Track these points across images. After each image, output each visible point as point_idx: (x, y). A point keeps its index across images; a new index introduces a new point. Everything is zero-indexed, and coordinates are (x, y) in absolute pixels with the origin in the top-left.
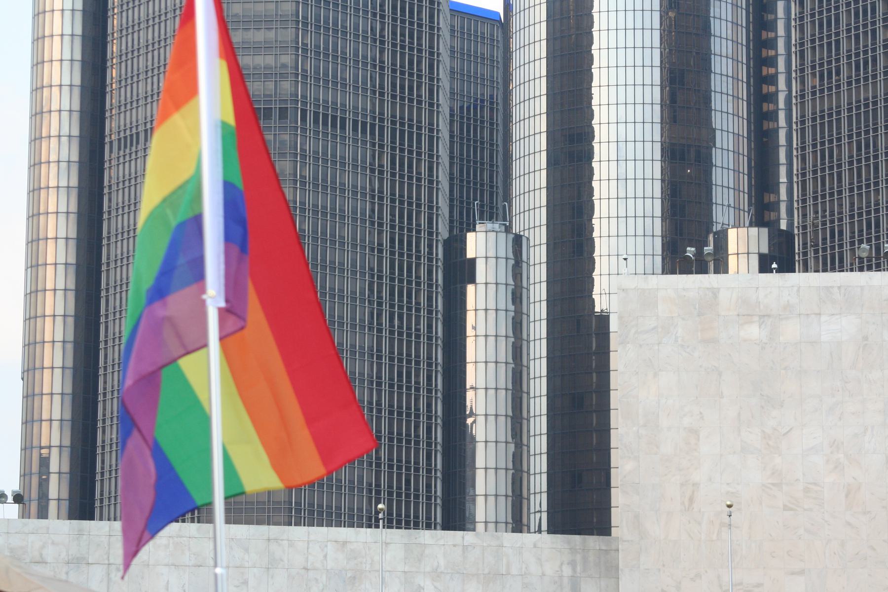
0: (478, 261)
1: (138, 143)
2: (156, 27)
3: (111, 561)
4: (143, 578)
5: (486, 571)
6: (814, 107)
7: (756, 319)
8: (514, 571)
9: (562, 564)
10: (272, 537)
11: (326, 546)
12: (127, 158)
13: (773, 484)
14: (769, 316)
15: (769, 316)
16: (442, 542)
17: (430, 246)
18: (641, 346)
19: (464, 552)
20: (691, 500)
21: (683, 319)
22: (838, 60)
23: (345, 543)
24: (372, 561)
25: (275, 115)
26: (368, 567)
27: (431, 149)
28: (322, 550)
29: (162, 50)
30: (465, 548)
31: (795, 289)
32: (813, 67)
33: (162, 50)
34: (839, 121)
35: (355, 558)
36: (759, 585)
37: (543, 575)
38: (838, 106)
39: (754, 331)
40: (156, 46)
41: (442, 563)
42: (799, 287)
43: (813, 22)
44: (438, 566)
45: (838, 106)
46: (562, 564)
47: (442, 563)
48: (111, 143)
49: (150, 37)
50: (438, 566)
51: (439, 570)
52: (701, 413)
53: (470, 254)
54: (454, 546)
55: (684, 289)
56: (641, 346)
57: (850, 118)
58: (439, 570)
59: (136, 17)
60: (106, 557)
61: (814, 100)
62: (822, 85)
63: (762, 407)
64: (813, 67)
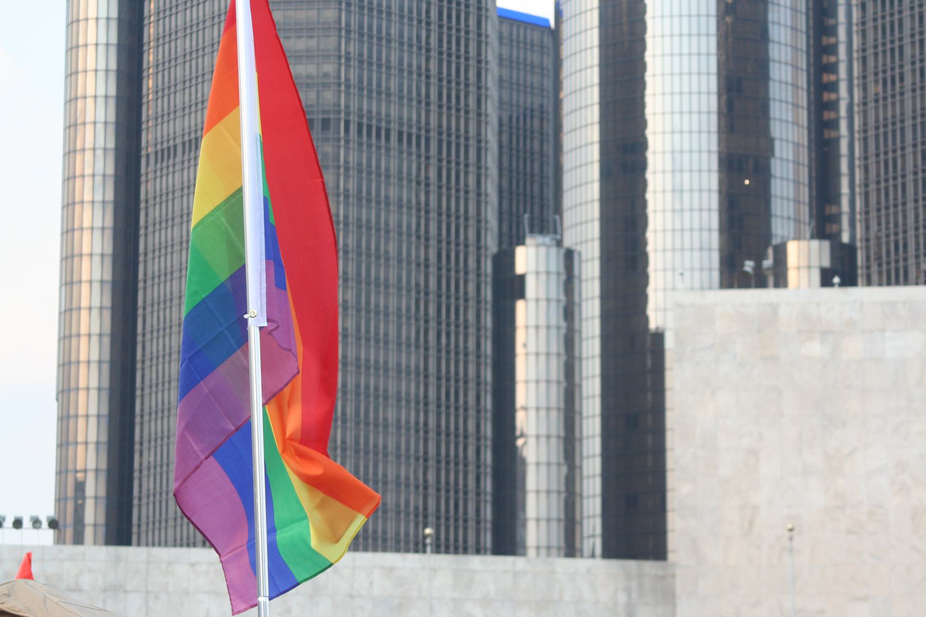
1: (175, 155)
6: (877, 115)
20: (751, 523)
30: (516, 574)
32: (876, 74)
39: (815, 348)
61: (877, 108)
62: (885, 91)
64: (876, 74)
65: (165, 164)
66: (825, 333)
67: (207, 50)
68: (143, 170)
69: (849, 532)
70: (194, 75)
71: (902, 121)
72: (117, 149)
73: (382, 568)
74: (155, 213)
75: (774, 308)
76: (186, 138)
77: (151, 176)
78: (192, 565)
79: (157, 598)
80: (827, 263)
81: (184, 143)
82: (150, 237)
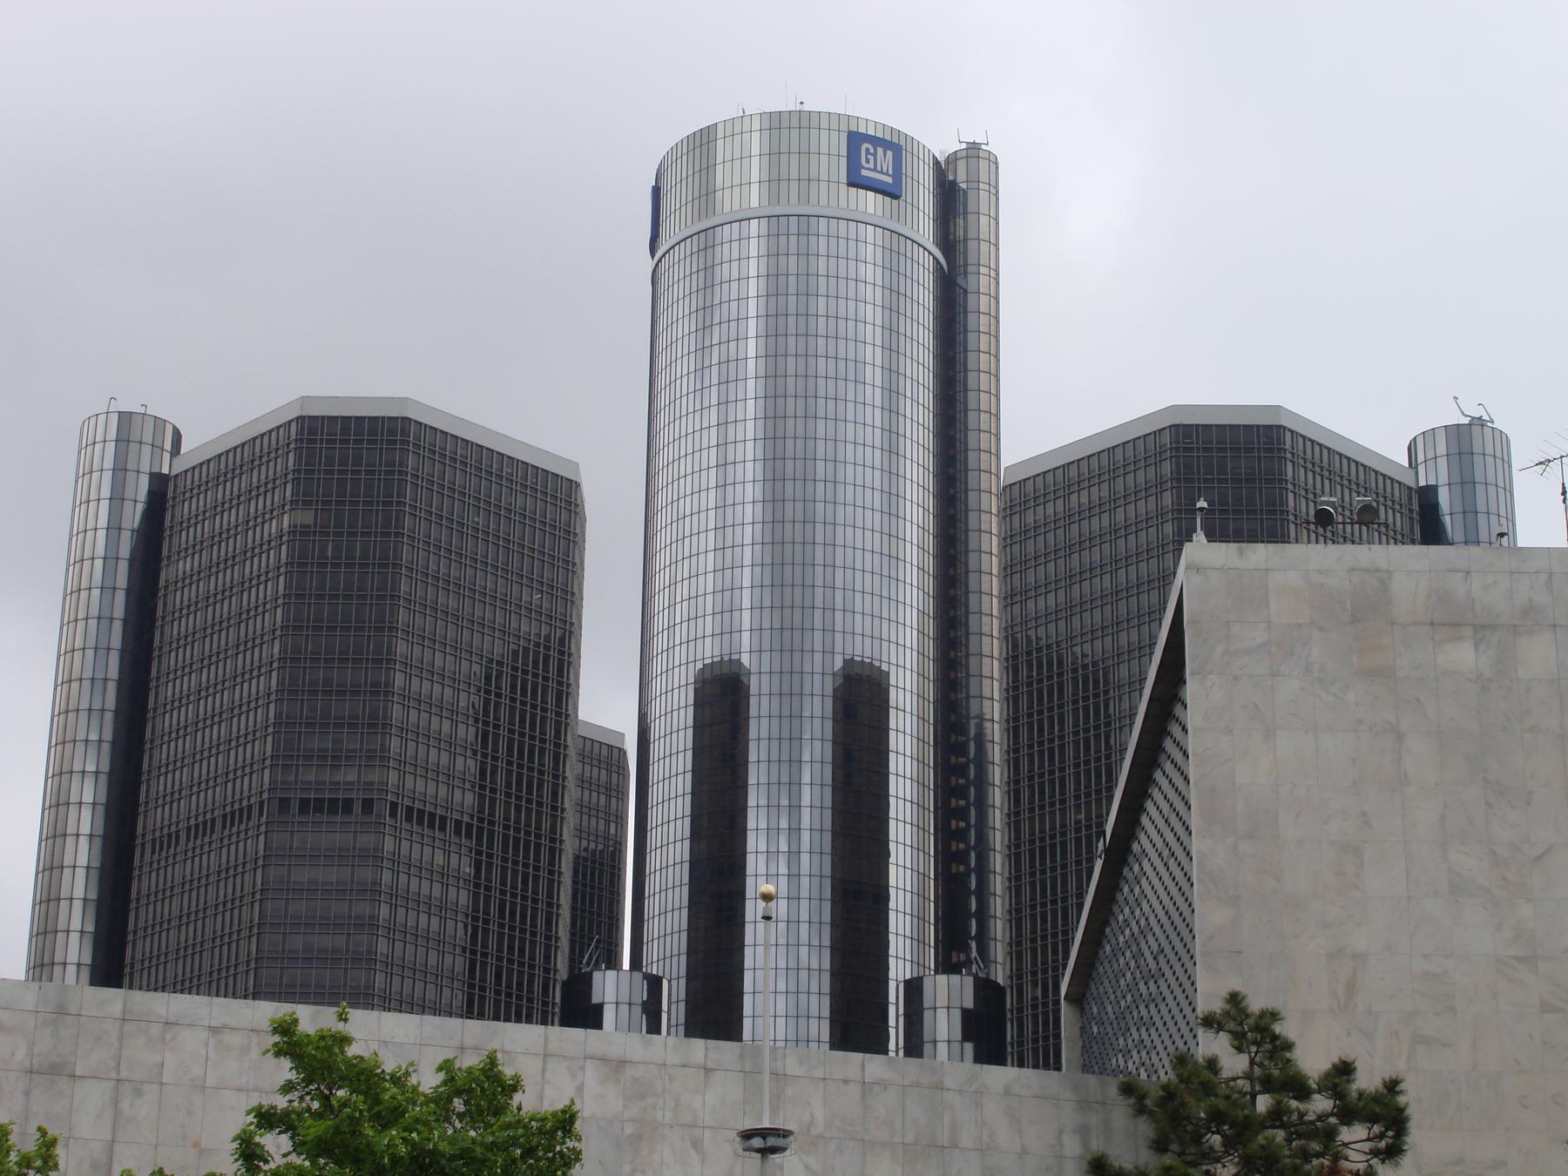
0: (606, 1008)
1: (177, 844)
2: (189, 959)
3: (124, 1074)
4: (190, 1113)
5: (910, 1137)
6: (1032, 828)
7: (1468, 631)
8: (966, 1140)
9: (1061, 1132)
10: (468, 1042)
11: (583, 1068)
12: (163, 863)
13: (1518, 959)
14: (1494, 627)
15: (1494, 627)
16: (819, 1074)
17: (546, 988)
18: (1236, 678)
19: (864, 1096)
20: (1351, 987)
21: (1321, 629)
22: (1062, 770)
23: (622, 1063)
24: (677, 1104)
25: (358, 807)
26: (669, 1115)
27: (552, 864)
28: (574, 1077)
29: (202, 891)
30: (866, 1087)
31: (1544, 577)
33: (202, 891)
34: (1063, 844)
35: (642, 1097)
36: (1499, 1164)
37: (1024, 1152)
38: (1063, 825)
39: (1463, 656)
40: (193, 917)
41: (819, 1115)
42: (1551, 575)
43: (1030, 725)
44: (811, 1123)
45: (1063, 825)
46: (1061, 1132)
47: (819, 1115)
48: (143, 845)
49: (180, 972)
50: (811, 1123)
51: (814, 1132)
52: (1364, 814)
53: (595, 1000)
54: (846, 1082)
55: (1320, 572)
56: (1236, 678)
57: (1078, 840)
58: (814, 1132)
59: (166, 911)
60: (112, 1063)
61: (1032, 819)
63: (1488, 804)
65: (164, 854)
66: (1483, 630)
67: (211, 879)
68: (137, 862)
69: (1546, 1007)
70: (193, 909)
71: (1063, 834)
72: (111, 774)
73: (603, 1060)
74: (163, 754)
75: (1383, 578)
76: (192, 822)
77: (146, 869)
78: (214, 1030)
79: (138, 1093)
80: (969, 1003)
81: (189, 829)
82: (142, 911)
